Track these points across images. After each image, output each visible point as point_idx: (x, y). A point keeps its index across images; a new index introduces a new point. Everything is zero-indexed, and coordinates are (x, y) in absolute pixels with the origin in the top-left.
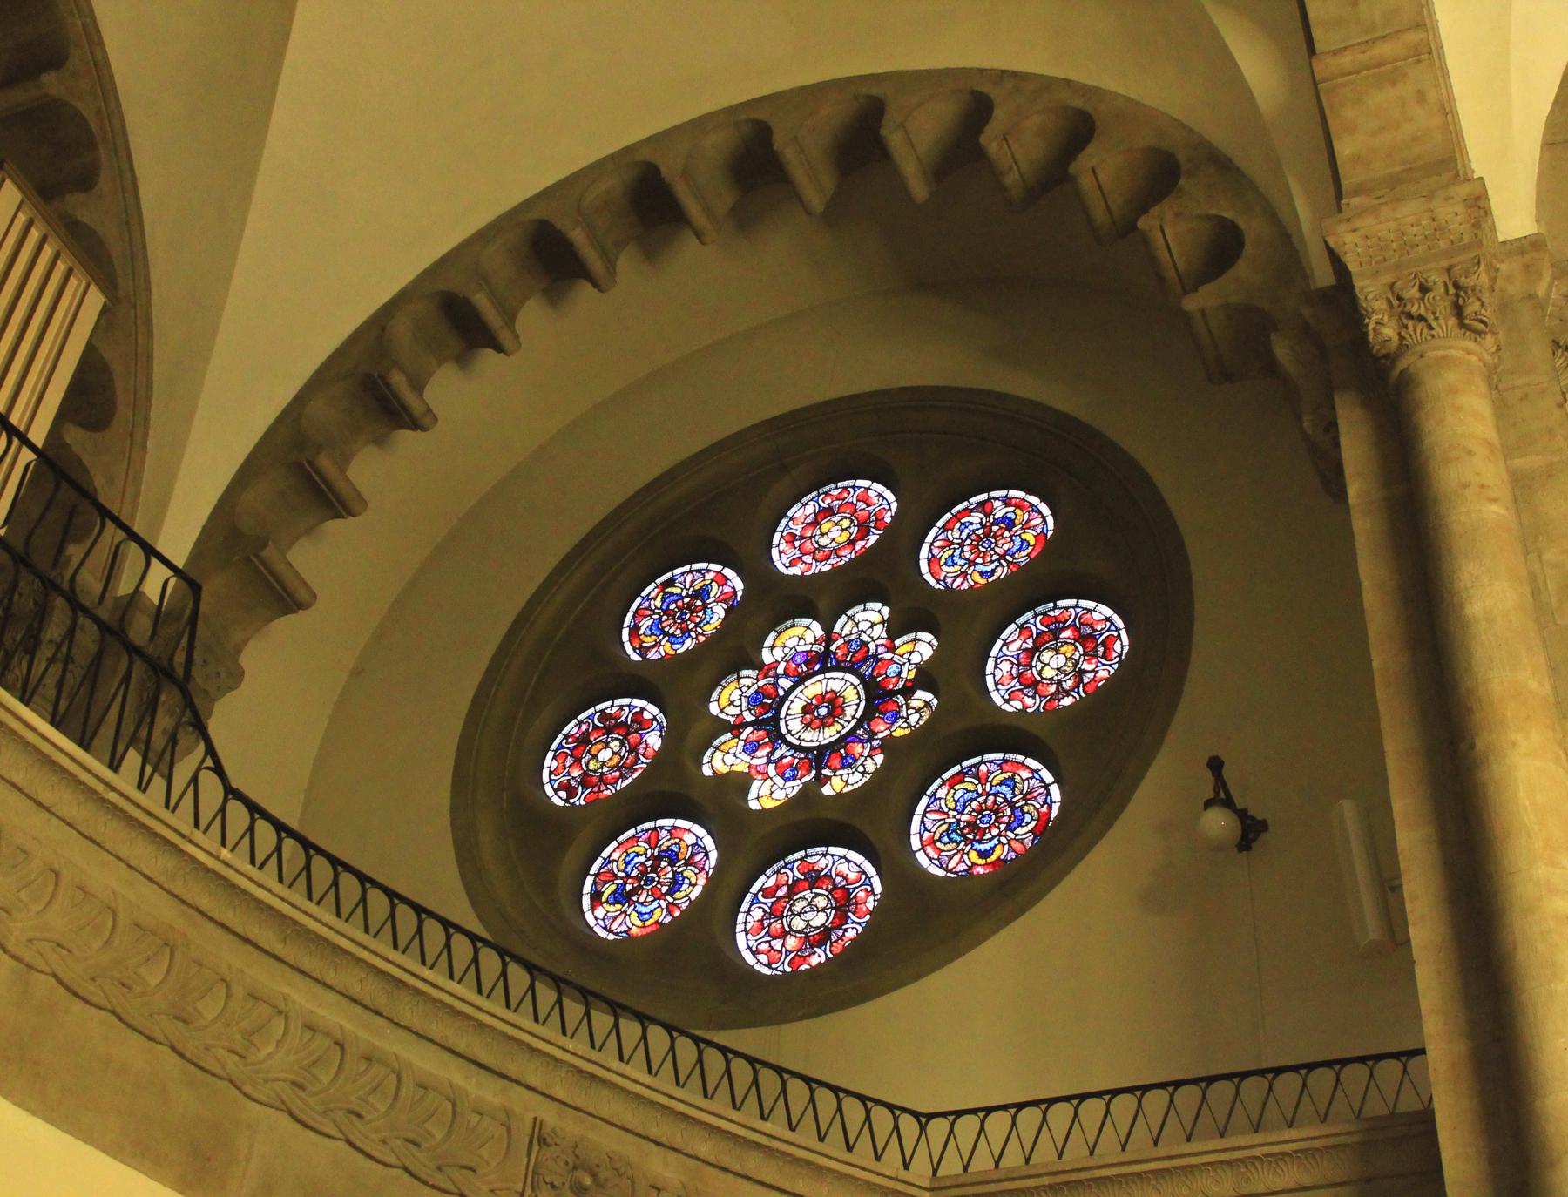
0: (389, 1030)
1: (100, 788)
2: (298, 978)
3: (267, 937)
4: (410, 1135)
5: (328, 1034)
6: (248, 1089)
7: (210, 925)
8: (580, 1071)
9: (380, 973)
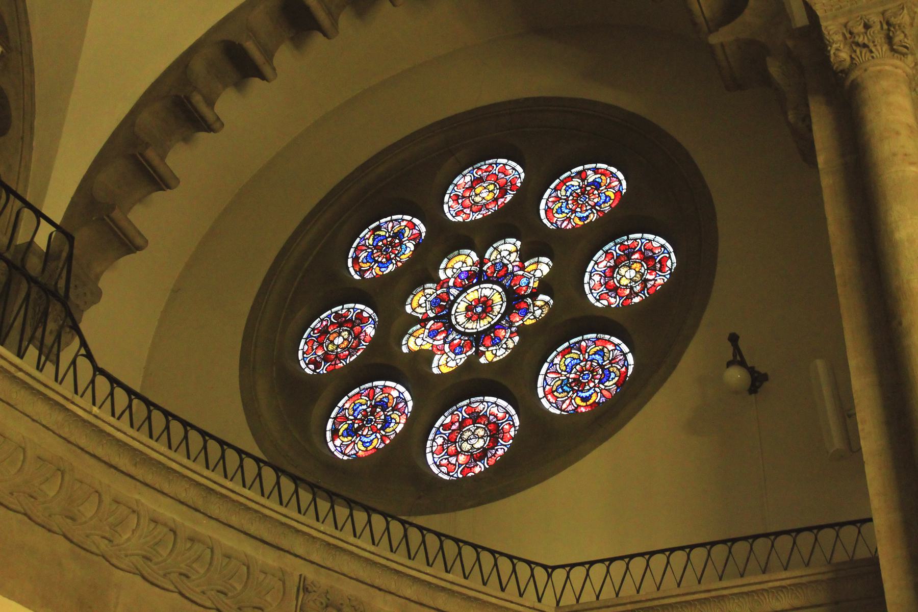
0: (205, 521)
1: (12, 370)
2: (145, 489)
3: (124, 462)
4: (219, 588)
5: (165, 525)
6: (114, 561)
7: (87, 456)
8: (329, 544)
9: (198, 484)
